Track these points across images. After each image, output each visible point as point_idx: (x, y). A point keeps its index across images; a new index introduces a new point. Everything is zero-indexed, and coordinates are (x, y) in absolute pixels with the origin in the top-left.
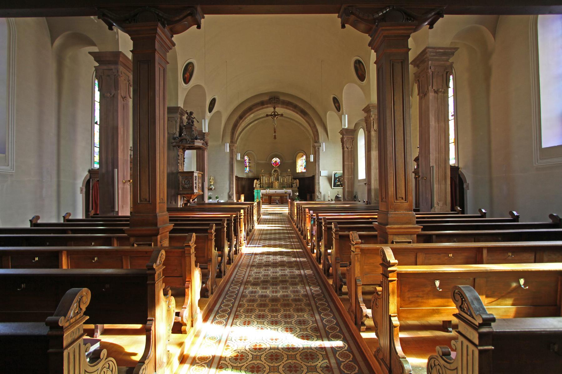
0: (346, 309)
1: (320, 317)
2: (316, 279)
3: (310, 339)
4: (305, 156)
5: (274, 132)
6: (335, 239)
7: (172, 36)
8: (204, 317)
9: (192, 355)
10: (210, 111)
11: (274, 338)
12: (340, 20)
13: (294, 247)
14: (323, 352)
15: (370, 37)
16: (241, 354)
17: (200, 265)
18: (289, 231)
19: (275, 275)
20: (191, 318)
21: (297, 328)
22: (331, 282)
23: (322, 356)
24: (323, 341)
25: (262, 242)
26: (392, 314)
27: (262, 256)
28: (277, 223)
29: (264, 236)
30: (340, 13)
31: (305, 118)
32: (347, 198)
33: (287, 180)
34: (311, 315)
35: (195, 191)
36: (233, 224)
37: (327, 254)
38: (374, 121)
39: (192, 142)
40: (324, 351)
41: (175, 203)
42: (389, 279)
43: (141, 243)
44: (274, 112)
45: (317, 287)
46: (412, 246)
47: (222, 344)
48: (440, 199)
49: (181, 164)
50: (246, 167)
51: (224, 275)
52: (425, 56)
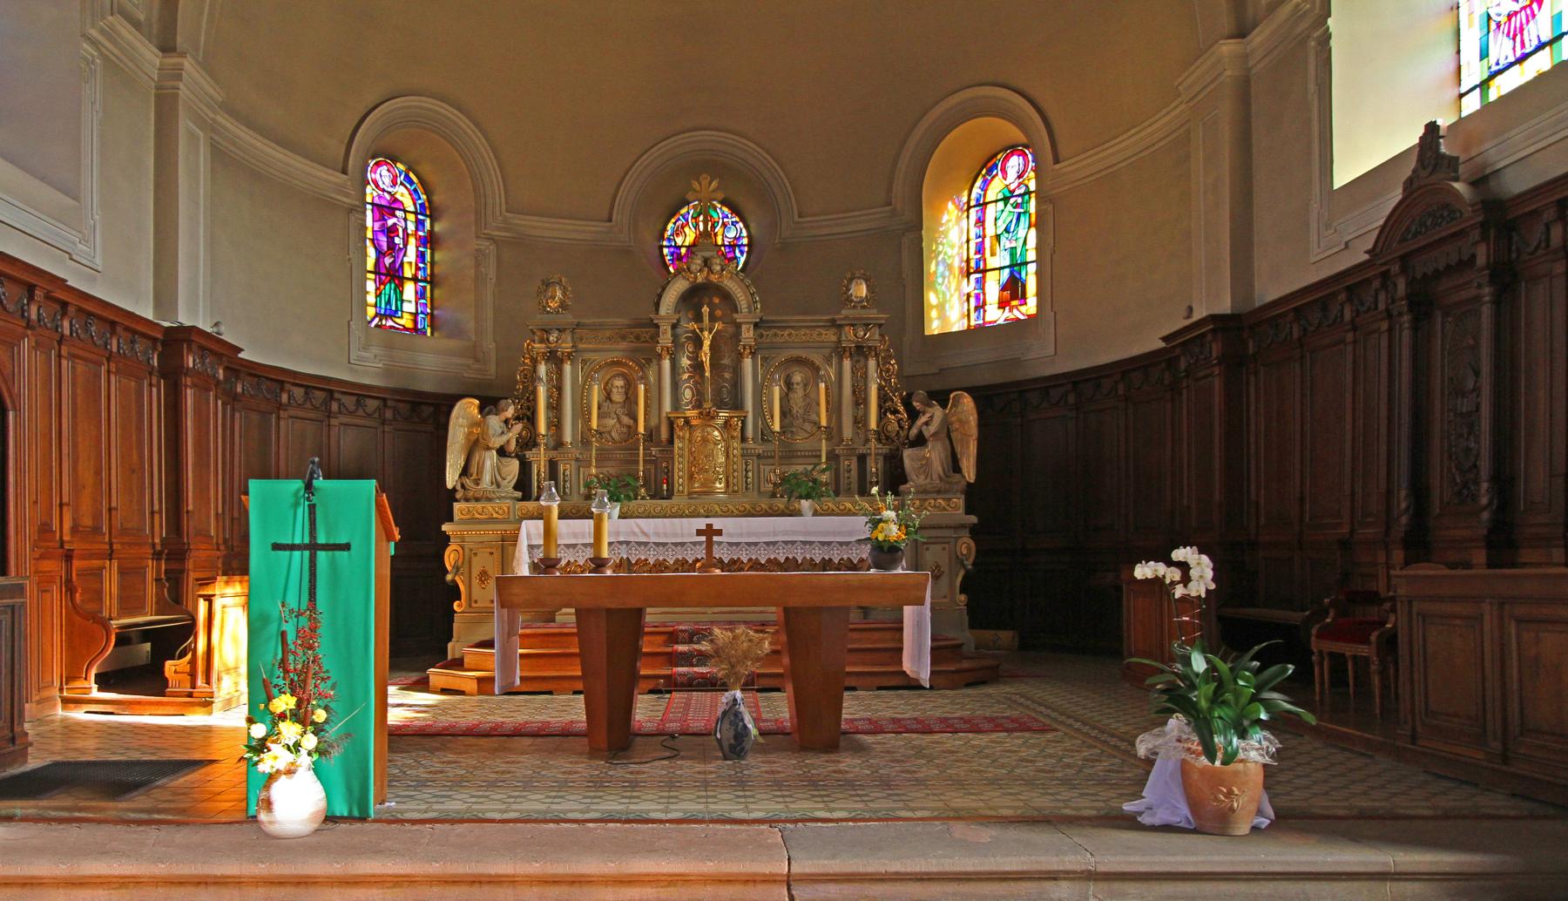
33: (835, 409)
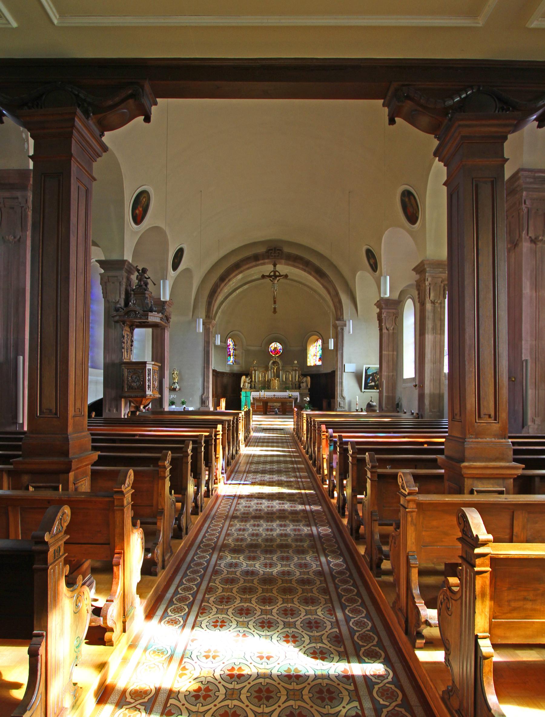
0: (389, 603)
1: (344, 614)
2: (337, 542)
3: (326, 658)
4: (320, 340)
5: (273, 302)
6: (371, 480)
7: (102, 135)
8: (148, 611)
9: (120, 685)
10: (175, 268)
11: (265, 655)
12: (386, 110)
13: (301, 486)
14: (350, 685)
15: (438, 140)
16: (206, 686)
17: (141, 523)
18: (293, 459)
19: (269, 535)
20: (122, 617)
21: (305, 636)
22: (362, 550)
23: (347, 693)
24: (349, 662)
25: (251, 476)
26: (480, 632)
27: (250, 501)
28: (275, 444)
29: (253, 467)
30: (388, 98)
31: (322, 281)
32: (385, 407)
33: (292, 378)
34: (329, 610)
35: (147, 393)
36: (203, 449)
37: (355, 502)
38: (432, 288)
40: (352, 684)
41: (117, 410)
42: (476, 569)
43: (41, 485)
44: (275, 272)
45: (338, 558)
46: (506, 499)
47: (175, 663)
48: (537, 413)
50: (230, 355)
51: (187, 534)
52: (517, 183)
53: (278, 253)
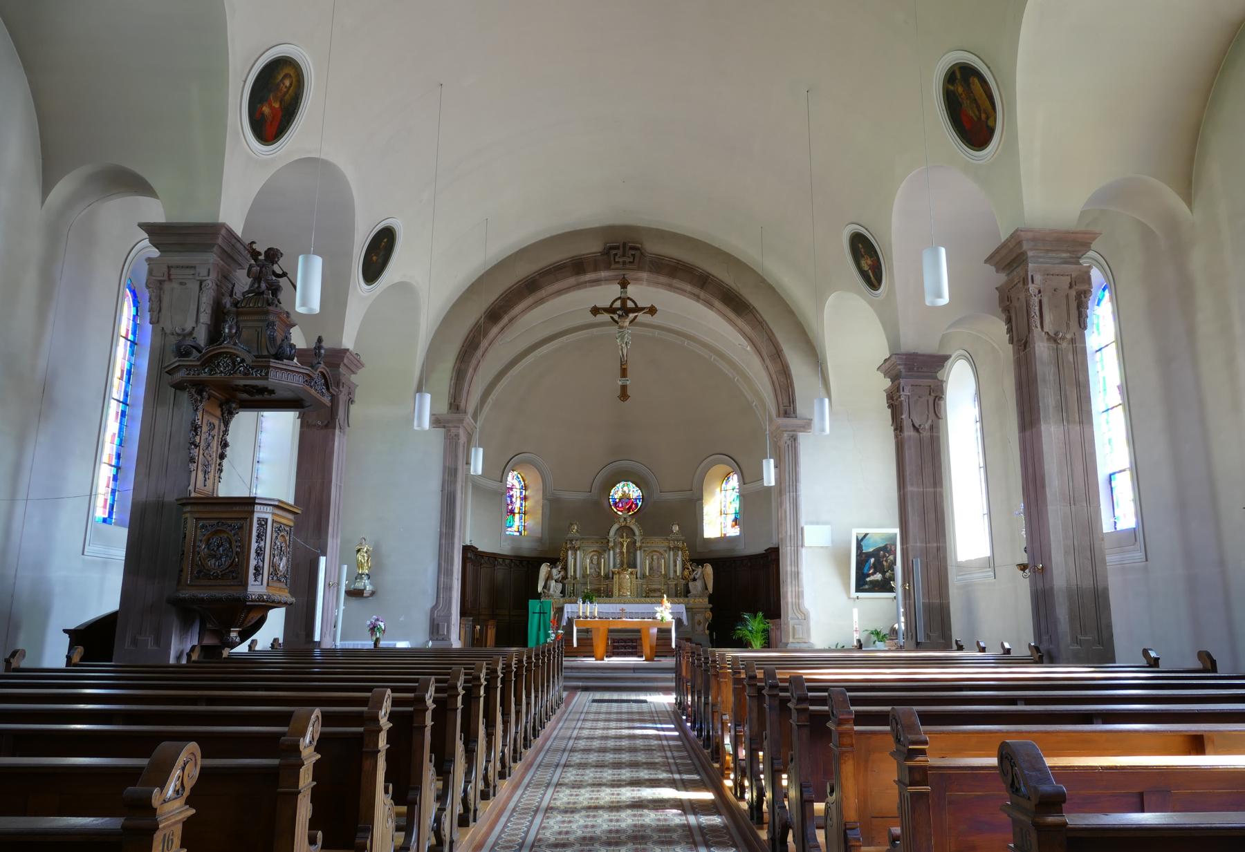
4: (735, 477)
5: (619, 372)
33: (667, 567)
38: (1045, 301)
39: (260, 368)
41: (157, 642)
44: (624, 300)
49: (206, 465)
53: (634, 255)
